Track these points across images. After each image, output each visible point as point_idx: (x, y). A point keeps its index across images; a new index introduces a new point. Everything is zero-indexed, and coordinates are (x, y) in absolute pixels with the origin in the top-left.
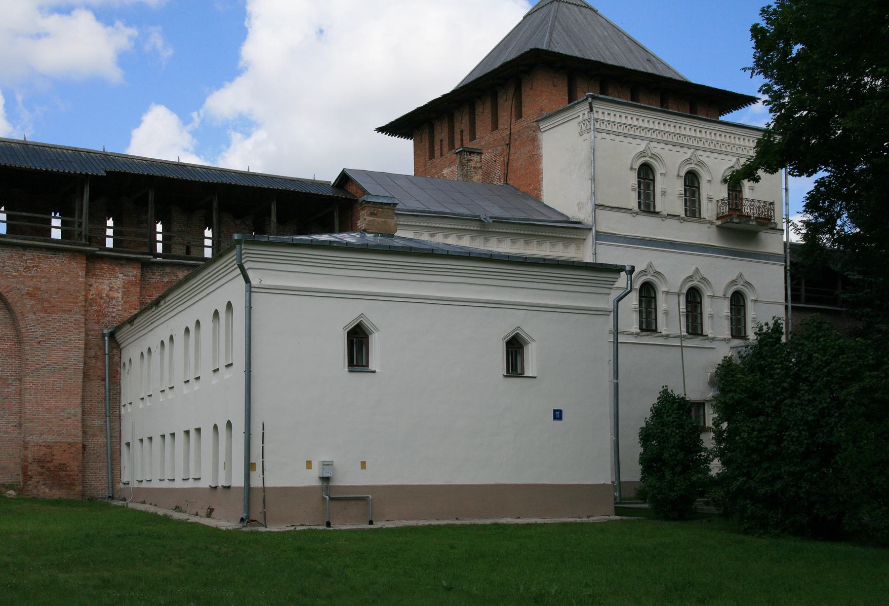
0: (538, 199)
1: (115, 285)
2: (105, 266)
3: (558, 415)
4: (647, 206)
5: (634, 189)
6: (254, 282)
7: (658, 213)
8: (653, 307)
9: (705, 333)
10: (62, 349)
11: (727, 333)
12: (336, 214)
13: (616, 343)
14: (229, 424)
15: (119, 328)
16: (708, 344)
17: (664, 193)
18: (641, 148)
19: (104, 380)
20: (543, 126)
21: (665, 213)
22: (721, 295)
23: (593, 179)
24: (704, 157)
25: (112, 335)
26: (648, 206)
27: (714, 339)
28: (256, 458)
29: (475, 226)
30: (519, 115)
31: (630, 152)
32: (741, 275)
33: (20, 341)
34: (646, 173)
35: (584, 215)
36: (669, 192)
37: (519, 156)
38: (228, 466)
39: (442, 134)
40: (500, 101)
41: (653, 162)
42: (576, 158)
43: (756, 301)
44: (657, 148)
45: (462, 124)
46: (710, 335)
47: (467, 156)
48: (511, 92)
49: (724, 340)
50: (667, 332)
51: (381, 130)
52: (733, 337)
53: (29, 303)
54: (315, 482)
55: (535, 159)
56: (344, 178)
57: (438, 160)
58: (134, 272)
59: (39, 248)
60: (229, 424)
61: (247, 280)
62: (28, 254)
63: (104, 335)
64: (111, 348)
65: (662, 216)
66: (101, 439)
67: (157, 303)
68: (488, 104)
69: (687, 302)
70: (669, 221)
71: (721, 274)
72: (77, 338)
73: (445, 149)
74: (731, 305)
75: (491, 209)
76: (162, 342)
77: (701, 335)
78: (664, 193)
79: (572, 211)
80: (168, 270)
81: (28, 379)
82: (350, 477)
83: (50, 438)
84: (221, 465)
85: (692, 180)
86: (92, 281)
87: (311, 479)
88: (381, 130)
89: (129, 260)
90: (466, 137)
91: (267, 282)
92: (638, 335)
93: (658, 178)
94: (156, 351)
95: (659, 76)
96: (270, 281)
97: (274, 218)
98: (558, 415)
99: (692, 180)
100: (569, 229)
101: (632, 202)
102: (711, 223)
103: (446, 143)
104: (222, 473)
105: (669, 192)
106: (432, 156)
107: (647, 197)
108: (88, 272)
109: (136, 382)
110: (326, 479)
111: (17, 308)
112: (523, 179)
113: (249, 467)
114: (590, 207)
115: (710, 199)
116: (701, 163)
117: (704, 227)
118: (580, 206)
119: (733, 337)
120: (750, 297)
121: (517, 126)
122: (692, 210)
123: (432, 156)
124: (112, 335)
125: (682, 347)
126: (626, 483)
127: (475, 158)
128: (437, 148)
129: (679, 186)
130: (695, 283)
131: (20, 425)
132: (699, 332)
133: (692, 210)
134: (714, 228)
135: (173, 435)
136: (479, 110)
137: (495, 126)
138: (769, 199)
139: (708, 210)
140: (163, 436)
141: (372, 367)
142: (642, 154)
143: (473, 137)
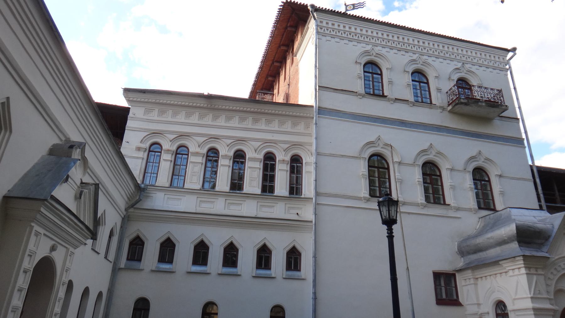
5: (360, 78)
7: (386, 96)
8: (489, 189)
9: (447, 203)
11: (472, 203)
13: (157, 174)
16: (451, 213)
21: (393, 97)
22: (461, 167)
27: (458, 209)
32: (480, 153)
36: (398, 83)
43: (500, 176)
46: (452, 205)
49: (470, 210)
50: (456, 205)
52: (480, 208)
65: (389, 100)
74: (424, 174)
77: (445, 204)
92: (368, 200)
102: (443, 109)
115: (439, 90)
116: (425, 63)
119: (480, 208)
120: (493, 173)
125: (179, 176)
126: (125, 265)
132: (492, 207)
138: (122, 91)
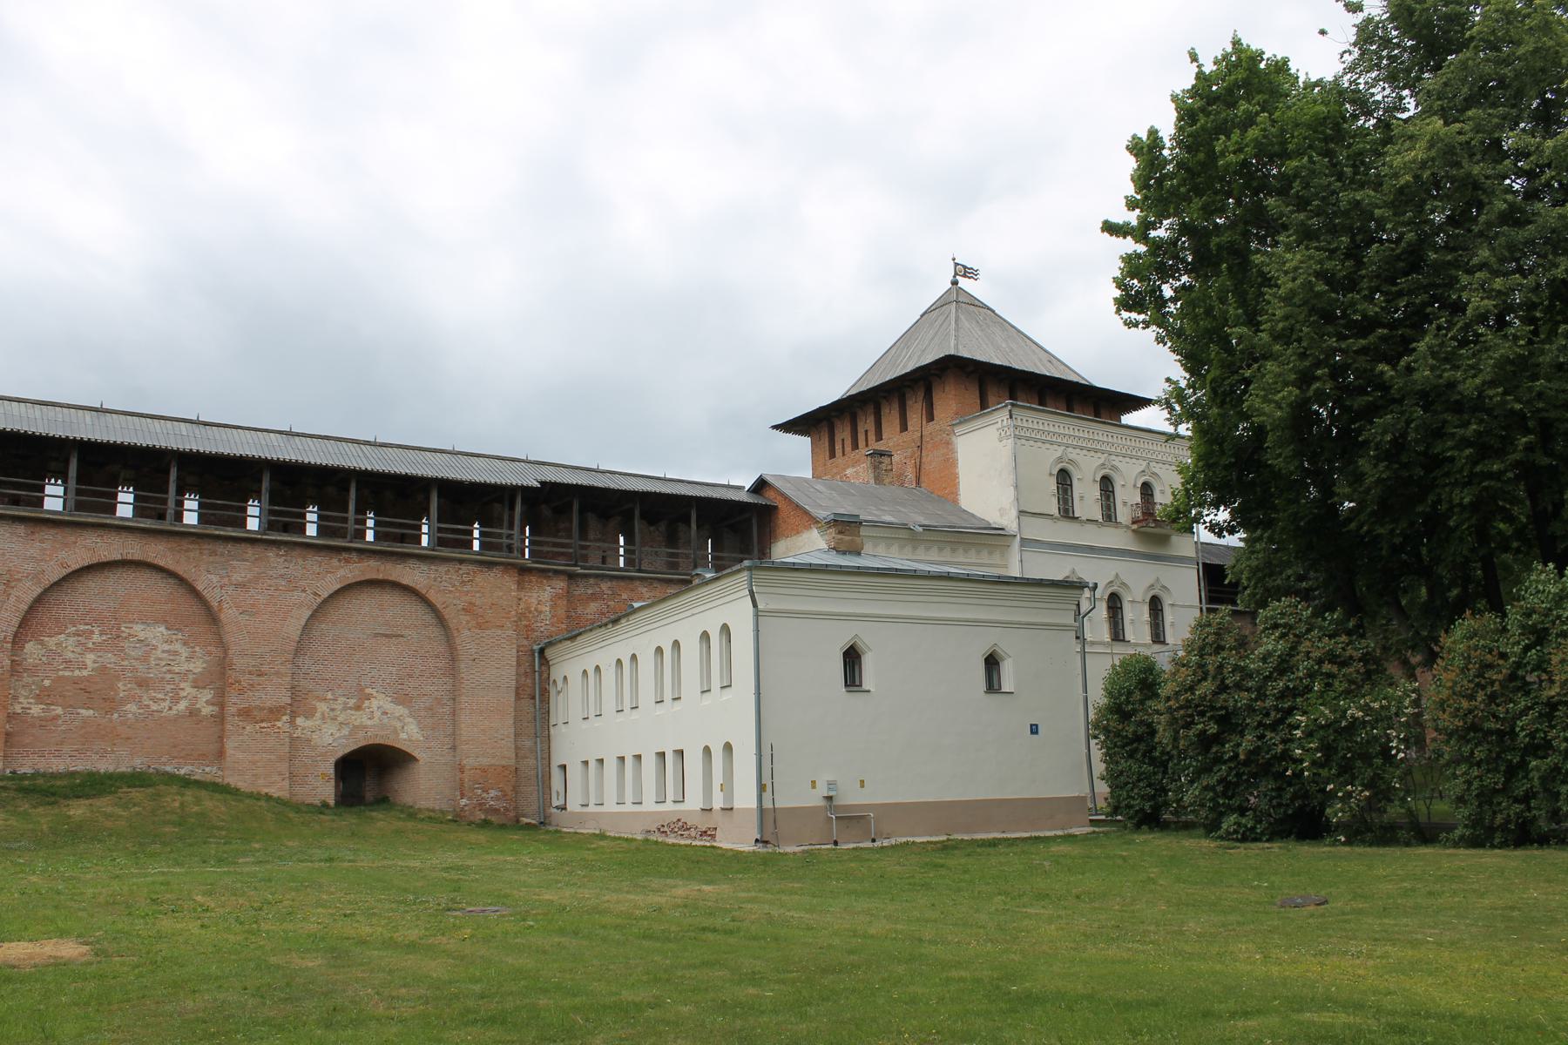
0: (955, 502)
1: (544, 597)
2: (534, 579)
3: (1034, 729)
4: (1067, 513)
6: (760, 607)
10: (493, 667)
12: (754, 521)
14: (728, 748)
15: (550, 644)
17: (1082, 498)
18: (1059, 454)
19: (533, 698)
20: (958, 430)
23: (1016, 487)
24: (1116, 461)
25: (542, 651)
26: (1066, 511)
28: (766, 780)
29: (903, 534)
30: (931, 418)
31: (1047, 459)
33: (453, 659)
34: (1064, 478)
35: (1009, 521)
36: (1087, 498)
37: (932, 460)
38: (727, 787)
39: (843, 434)
40: (909, 403)
41: (1070, 468)
42: (989, 465)
44: (1073, 454)
45: (866, 424)
47: (878, 459)
48: (921, 394)
51: (776, 427)
53: (464, 618)
54: (822, 803)
55: (950, 463)
56: (761, 485)
57: (839, 459)
58: (560, 584)
59: (461, 561)
60: (728, 748)
61: (755, 605)
62: (464, 568)
63: (533, 651)
64: (541, 665)
66: (532, 762)
67: (615, 622)
68: (896, 406)
69: (1109, 608)
70: (1089, 526)
71: (1138, 580)
72: (509, 655)
73: (848, 448)
75: (917, 519)
76: (619, 662)
78: (1082, 498)
79: (994, 519)
80: (592, 581)
81: (464, 699)
82: (852, 797)
83: (485, 761)
84: (769, 788)
85: (1106, 484)
86: (522, 594)
87: (814, 799)
88: (776, 427)
89: (556, 572)
90: (872, 437)
91: (772, 606)
93: (1075, 483)
94: (609, 675)
95: (1077, 383)
96: (774, 605)
97: (694, 526)
98: (1034, 729)
99: (1106, 484)
100: (992, 537)
101: (1053, 508)
103: (848, 442)
104: (629, 797)
105: (1087, 498)
106: (832, 455)
107: (1066, 501)
108: (520, 586)
109: (569, 704)
110: (829, 798)
111: (452, 624)
112: (939, 481)
113: (761, 788)
114: (1014, 513)
116: (1114, 468)
117: (1120, 531)
118: (1002, 511)
120: (1167, 602)
121: (929, 428)
122: (1109, 515)
123: (832, 455)
124: (542, 651)
127: (886, 460)
128: (838, 447)
129: (1096, 492)
130: (1114, 588)
131: (454, 748)
133: (1109, 515)
134: (1130, 533)
135: (638, 757)
136: (885, 411)
137: (904, 428)
139: (1123, 515)
140: (586, 763)
141: (865, 686)
142: (1060, 460)
143: (879, 437)
